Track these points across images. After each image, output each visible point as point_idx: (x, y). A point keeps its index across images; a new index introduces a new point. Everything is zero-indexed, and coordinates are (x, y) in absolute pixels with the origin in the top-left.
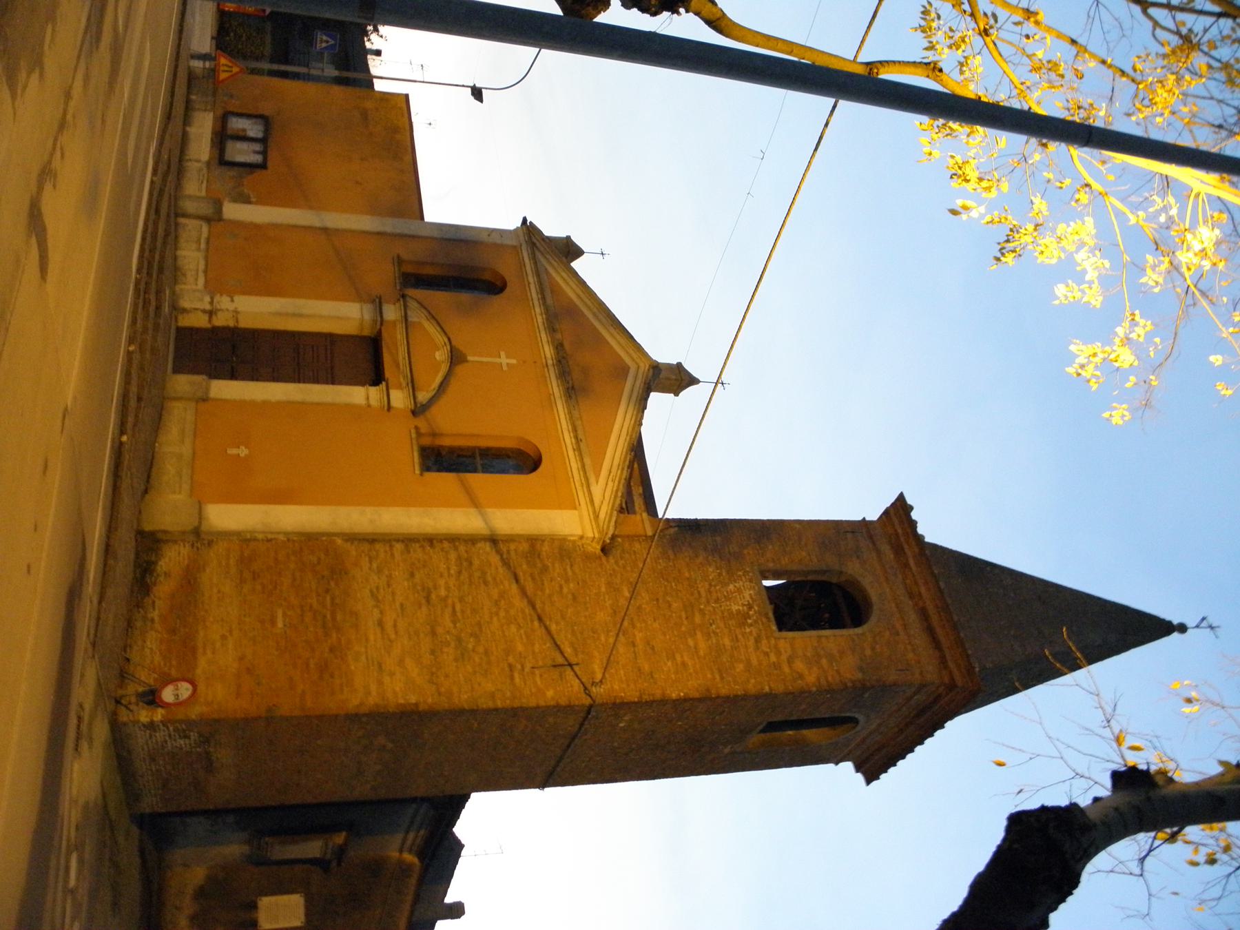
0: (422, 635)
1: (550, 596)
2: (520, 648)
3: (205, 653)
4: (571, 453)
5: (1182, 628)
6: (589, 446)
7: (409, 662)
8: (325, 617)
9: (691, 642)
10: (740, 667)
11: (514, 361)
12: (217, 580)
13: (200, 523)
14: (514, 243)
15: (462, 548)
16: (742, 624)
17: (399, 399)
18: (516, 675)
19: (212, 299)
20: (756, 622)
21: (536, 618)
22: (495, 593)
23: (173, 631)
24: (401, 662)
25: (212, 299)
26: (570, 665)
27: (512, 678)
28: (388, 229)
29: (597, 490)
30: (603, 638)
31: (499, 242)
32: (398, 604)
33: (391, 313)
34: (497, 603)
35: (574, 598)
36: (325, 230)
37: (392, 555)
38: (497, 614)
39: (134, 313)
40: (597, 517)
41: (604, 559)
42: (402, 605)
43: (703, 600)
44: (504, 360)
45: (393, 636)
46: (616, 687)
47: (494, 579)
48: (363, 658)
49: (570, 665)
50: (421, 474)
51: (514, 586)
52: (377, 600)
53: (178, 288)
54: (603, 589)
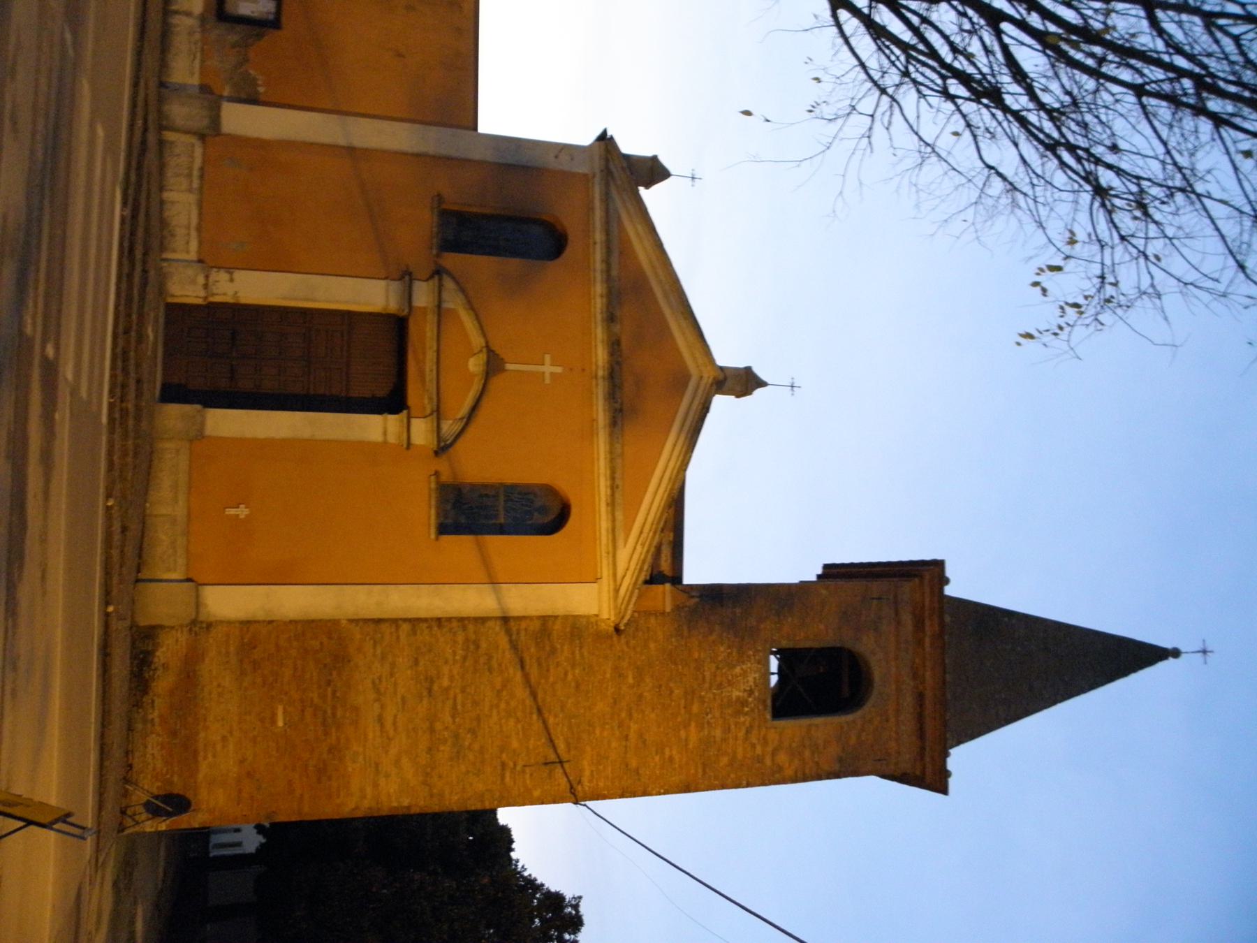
0: (420, 733)
1: (554, 684)
2: (515, 744)
3: (205, 758)
4: (603, 508)
5: (1176, 653)
6: (623, 494)
7: (405, 761)
8: (325, 712)
9: (683, 734)
10: (724, 760)
11: (558, 370)
12: (217, 674)
13: (198, 613)
14: (583, 169)
15: (471, 627)
16: (738, 713)
17: (421, 432)
18: (508, 775)
19: (207, 277)
20: (752, 710)
21: (535, 710)
22: (498, 681)
23: (174, 734)
24: (397, 762)
25: (207, 277)
26: (561, 762)
27: (503, 777)
28: (430, 149)
29: (623, 555)
30: (598, 732)
31: (566, 168)
32: (399, 696)
33: (423, 295)
34: (499, 692)
35: (577, 686)
36: (351, 150)
37: (398, 638)
38: (497, 706)
39: (113, 368)
40: (617, 591)
41: (615, 638)
42: (403, 698)
43: (707, 685)
44: (548, 369)
45: (391, 733)
46: (601, 784)
47: (500, 665)
48: (361, 758)
49: (561, 762)
50: (437, 539)
51: (519, 674)
52: (378, 691)
53: (166, 195)
54: (608, 676)
